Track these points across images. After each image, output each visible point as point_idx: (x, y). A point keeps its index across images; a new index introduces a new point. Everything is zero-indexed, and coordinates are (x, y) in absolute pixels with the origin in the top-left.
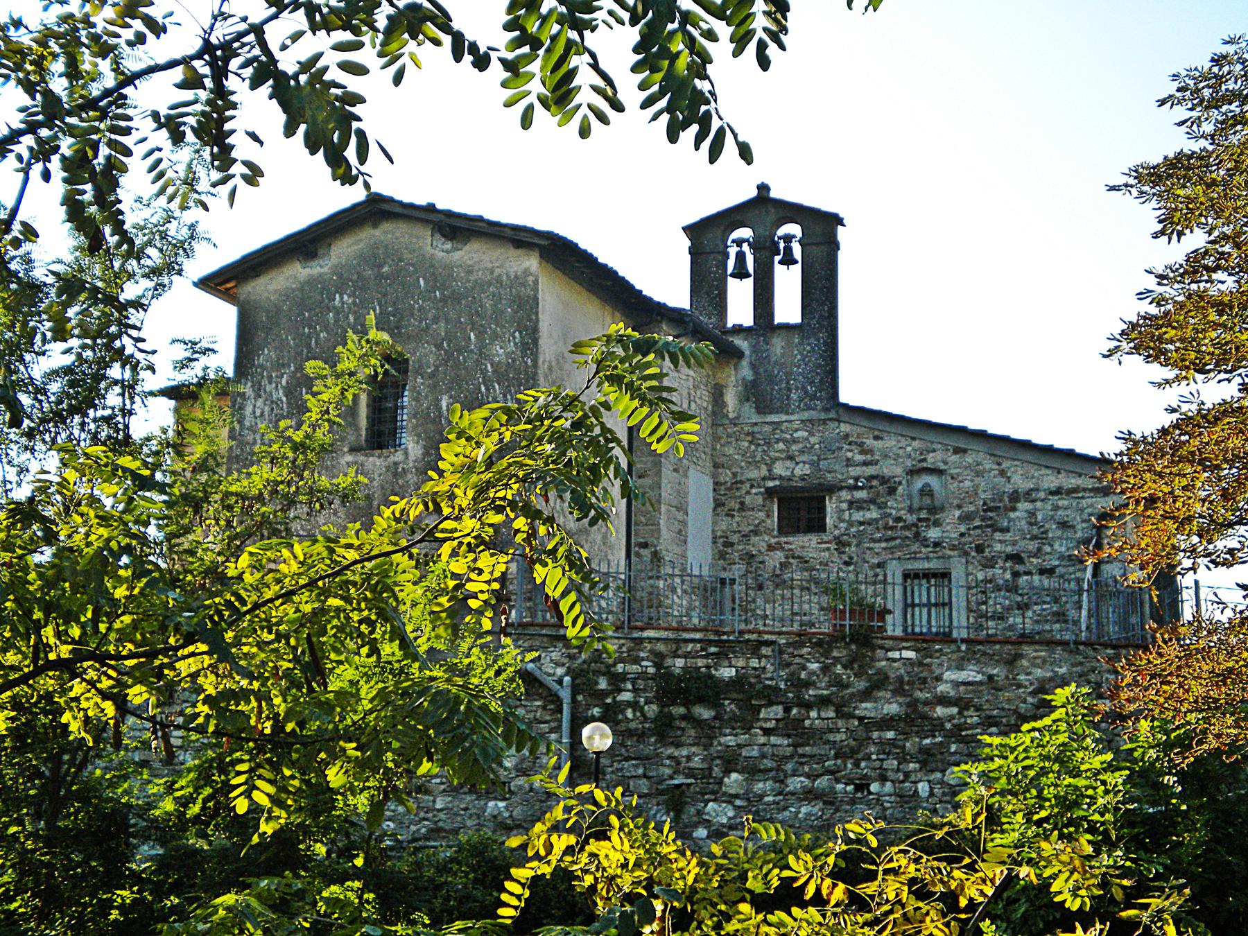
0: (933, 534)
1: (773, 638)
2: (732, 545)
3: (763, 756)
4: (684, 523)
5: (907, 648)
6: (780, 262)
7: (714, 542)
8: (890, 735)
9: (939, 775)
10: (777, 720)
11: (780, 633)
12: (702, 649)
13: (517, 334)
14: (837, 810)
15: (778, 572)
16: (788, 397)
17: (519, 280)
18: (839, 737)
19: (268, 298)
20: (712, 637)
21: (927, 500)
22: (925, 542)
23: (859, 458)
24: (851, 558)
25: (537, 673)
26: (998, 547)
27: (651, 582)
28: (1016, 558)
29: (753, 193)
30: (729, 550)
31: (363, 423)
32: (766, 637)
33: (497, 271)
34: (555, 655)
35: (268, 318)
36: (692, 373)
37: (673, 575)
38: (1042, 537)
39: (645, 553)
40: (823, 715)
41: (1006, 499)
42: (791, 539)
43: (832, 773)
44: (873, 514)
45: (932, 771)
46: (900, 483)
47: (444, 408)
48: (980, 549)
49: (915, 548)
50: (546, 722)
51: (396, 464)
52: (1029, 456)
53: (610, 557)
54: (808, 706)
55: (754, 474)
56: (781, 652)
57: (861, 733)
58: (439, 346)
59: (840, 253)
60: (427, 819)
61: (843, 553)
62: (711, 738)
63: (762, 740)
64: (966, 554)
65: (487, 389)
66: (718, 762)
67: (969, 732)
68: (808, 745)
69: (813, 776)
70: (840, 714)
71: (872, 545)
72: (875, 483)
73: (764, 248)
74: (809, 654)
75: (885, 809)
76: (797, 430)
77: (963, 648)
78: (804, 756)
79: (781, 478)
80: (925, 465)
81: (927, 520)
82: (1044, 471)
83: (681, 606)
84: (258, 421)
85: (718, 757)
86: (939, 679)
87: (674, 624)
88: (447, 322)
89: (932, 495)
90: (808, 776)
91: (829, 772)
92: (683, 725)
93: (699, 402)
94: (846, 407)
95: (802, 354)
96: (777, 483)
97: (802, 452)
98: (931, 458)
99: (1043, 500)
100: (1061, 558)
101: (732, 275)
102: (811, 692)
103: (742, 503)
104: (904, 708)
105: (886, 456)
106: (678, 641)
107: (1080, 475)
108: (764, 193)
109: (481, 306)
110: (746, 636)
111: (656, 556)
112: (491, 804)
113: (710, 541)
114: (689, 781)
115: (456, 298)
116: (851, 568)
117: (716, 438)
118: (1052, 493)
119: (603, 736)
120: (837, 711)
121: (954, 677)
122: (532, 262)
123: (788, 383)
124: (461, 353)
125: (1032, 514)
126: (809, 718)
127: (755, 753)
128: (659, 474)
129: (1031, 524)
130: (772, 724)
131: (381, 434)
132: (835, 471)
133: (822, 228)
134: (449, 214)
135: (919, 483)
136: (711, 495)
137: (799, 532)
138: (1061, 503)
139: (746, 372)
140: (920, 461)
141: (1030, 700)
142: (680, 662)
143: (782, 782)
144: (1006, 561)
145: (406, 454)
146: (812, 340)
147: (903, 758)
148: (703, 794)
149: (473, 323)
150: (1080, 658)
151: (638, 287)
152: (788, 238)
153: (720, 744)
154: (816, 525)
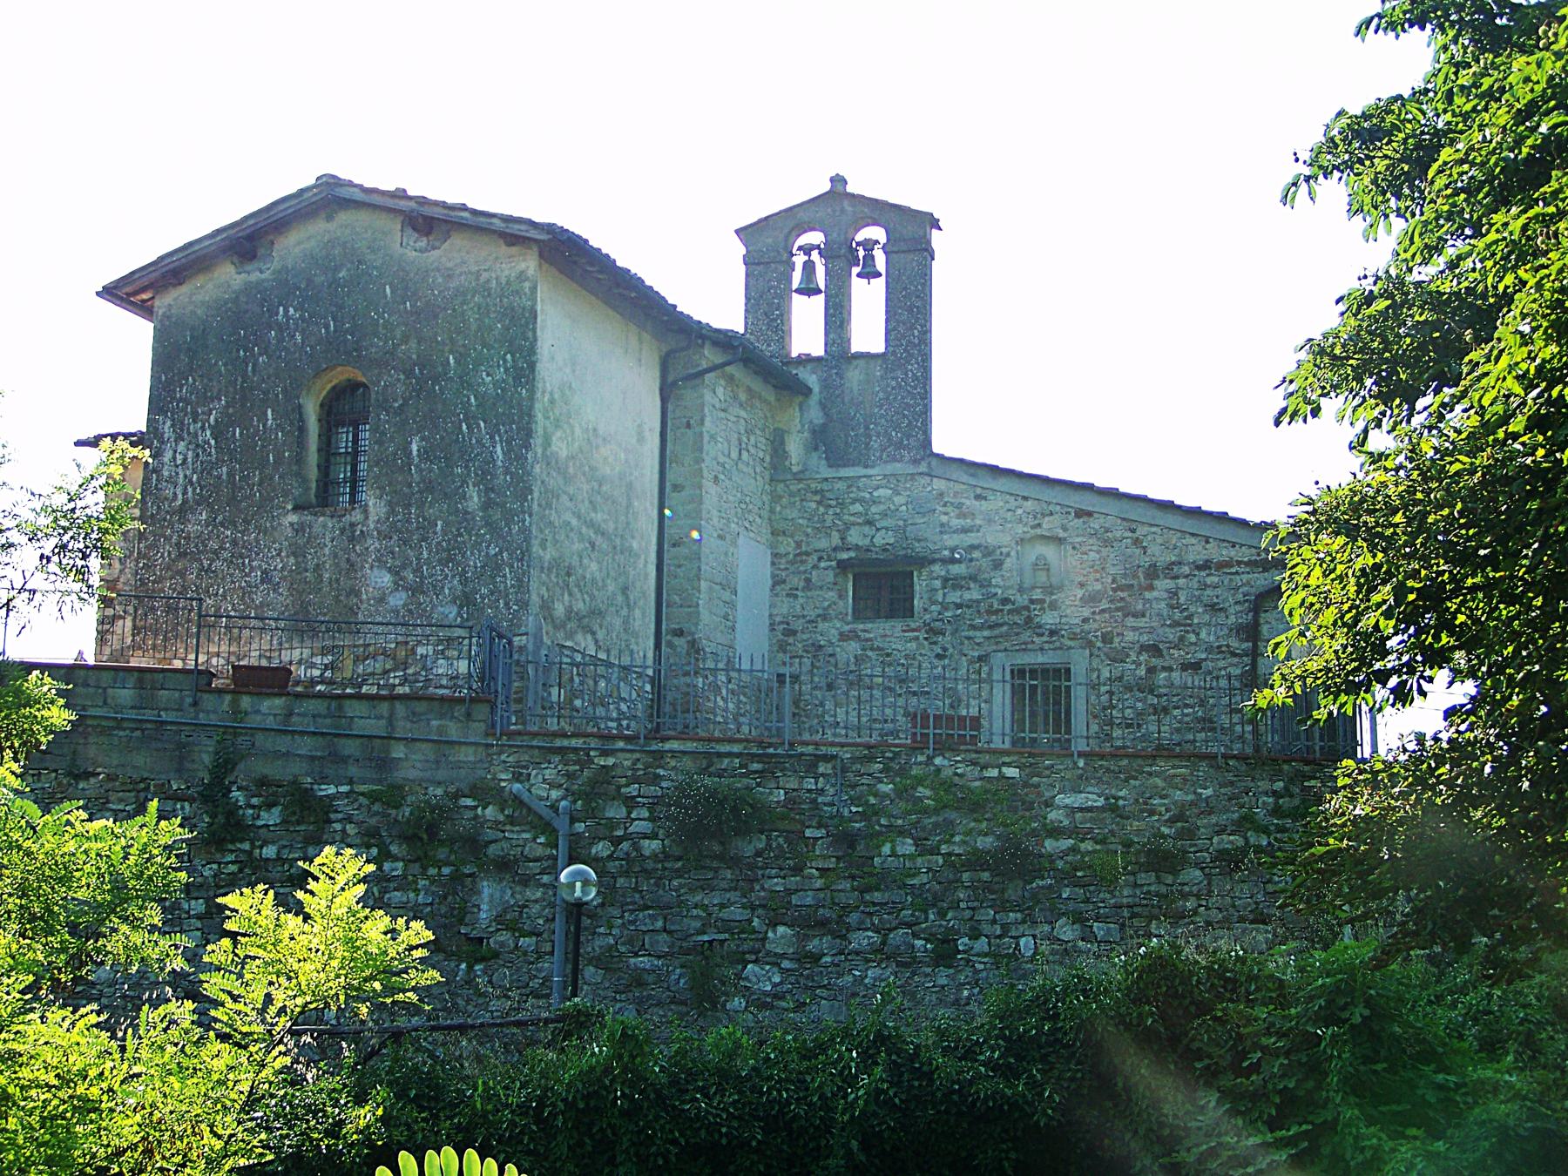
1: (834, 750)
2: (794, 633)
4: (732, 605)
5: (1008, 765)
6: (859, 275)
9: (1047, 928)
14: (914, 974)
15: (853, 667)
20: (754, 750)
22: (1038, 629)
24: (945, 649)
25: (525, 797)
26: (1130, 636)
27: (687, 679)
28: (1154, 650)
29: (827, 187)
30: (791, 640)
33: (485, 276)
34: (549, 773)
35: (192, 337)
36: (743, 414)
38: (1186, 624)
39: (680, 642)
42: (870, 626)
43: (909, 925)
46: (1008, 555)
47: (415, 453)
50: (536, 860)
51: (352, 525)
55: (823, 544)
56: (844, 770)
58: (409, 373)
59: (936, 265)
61: (935, 643)
66: (760, 911)
68: (878, 890)
71: (971, 633)
72: (976, 554)
75: (977, 972)
76: (877, 488)
77: (1081, 764)
80: (1039, 531)
81: (1042, 601)
83: (726, 710)
84: (180, 470)
86: (1049, 804)
87: (717, 734)
93: (752, 451)
94: (940, 457)
95: (885, 392)
96: (852, 554)
100: (1209, 649)
101: (798, 291)
103: (808, 581)
105: (990, 521)
108: (839, 187)
109: (464, 321)
110: (800, 749)
114: (722, 936)
117: (776, 498)
118: (1199, 568)
119: (586, 883)
122: (529, 263)
123: (867, 428)
127: (809, 901)
129: (1172, 607)
132: (926, 540)
133: (912, 234)
138: (1209, 580)
139: (815, 415)
143: (843, 938)
145: (366, 511)
150: (1230, 776)
151: (648, 283)
152: (869, 245)
153: (763, 888)
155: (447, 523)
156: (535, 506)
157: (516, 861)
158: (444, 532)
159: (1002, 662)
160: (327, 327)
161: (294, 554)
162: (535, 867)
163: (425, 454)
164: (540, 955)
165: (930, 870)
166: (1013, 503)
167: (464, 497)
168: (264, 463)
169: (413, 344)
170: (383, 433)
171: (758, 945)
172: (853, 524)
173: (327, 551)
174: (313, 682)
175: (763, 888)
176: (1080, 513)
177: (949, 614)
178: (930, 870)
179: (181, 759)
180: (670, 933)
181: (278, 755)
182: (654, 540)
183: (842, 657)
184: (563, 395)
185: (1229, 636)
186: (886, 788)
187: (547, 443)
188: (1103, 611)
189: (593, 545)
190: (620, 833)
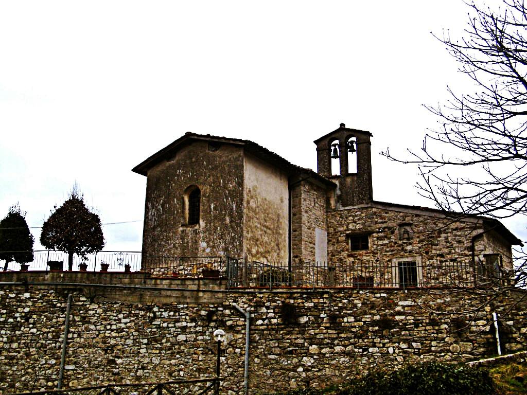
0: (409, 248)
1: (328, 290)
3: (325, 338)
5: (383, 293)
7: (328, 255)
14: (355, 360)
18: (354, 330)
22: (405, 251)
23: (380, 221)
24: (378, 258)
25: (237, 306)
26: (434, 252)
28: (442, 256)
29: (338, 127)
30: (334, 258)
31: (187, 216)
34: (244, 300)
36: (315, 193)
39: (297, 260)
40: (349, 320)
42: (355, 253)
44: (386, 241)
45: (395, 343)
46: (396, 229)
47: (212, 208)
48: (427, 253)
49: (402, 253)
51: (196, 230)
55: (341, 229)
58: (210, 186)
60: (196, 364)
61: (375, 257)
65: (226, 200)
67: (409, 326)
69: (345, 346)
71: (386, 253)
72: (386, 230)
74: (343, 296)
75: (375, 359)
76: (357, 212)
85: (307, 339)
86: (397, 305)
88: (213, 176)
90: (343, 346)
91: (351, 344)
95: (357, 183)
96: (350, 232)
97: (359, 220)
99: (450, 233)
100: (459, 255)
101: (333, 157)
103: (338, 240)
111: (301, 261)
116: (379, 262)
117: (328, 217)
118: (454, 230)
123: (353, 195)
124: (217, 187)
125: (446, 238)
126: (343, 322)
128: (301, 230)
129: (446, 242)
133: (364, 138)
136: (326, 238)
140: (403, 221)
143: (333, 348)
147: (382, 337)
148: (301, 354)
151: (289, 161)
152: (352, 142)
155: (221, 228)
156: (244, 221)
157: (235, 326)
158: (220, 230)
159: (395, 261)
160: (189, 174)
161: (182, 239)
162: (240, 328)
163: (215, 208)
164: (241, 355)
165: (359, 326)
166: (396, 214)
167: (225, 220)
168: (174, 214)
169: (212, 177)
170: (204, 203)
171: (306, 351)
172: (350, 223)
173: (190, 237)
174: (186, 275)
175: (308, 333)
176: (417, 215)
177: (379, 248)
178: (359, 326)
179: (141, 298)
180: (280, 348)
181: (167, 296)
182: (288, 230)
183: (348, 263)
184: (254, 189)
185: (465, 250)
186: (345, 301)
187: (248, 202)
188: (426, 244)
189: (266, 232)
190: (264, 317)
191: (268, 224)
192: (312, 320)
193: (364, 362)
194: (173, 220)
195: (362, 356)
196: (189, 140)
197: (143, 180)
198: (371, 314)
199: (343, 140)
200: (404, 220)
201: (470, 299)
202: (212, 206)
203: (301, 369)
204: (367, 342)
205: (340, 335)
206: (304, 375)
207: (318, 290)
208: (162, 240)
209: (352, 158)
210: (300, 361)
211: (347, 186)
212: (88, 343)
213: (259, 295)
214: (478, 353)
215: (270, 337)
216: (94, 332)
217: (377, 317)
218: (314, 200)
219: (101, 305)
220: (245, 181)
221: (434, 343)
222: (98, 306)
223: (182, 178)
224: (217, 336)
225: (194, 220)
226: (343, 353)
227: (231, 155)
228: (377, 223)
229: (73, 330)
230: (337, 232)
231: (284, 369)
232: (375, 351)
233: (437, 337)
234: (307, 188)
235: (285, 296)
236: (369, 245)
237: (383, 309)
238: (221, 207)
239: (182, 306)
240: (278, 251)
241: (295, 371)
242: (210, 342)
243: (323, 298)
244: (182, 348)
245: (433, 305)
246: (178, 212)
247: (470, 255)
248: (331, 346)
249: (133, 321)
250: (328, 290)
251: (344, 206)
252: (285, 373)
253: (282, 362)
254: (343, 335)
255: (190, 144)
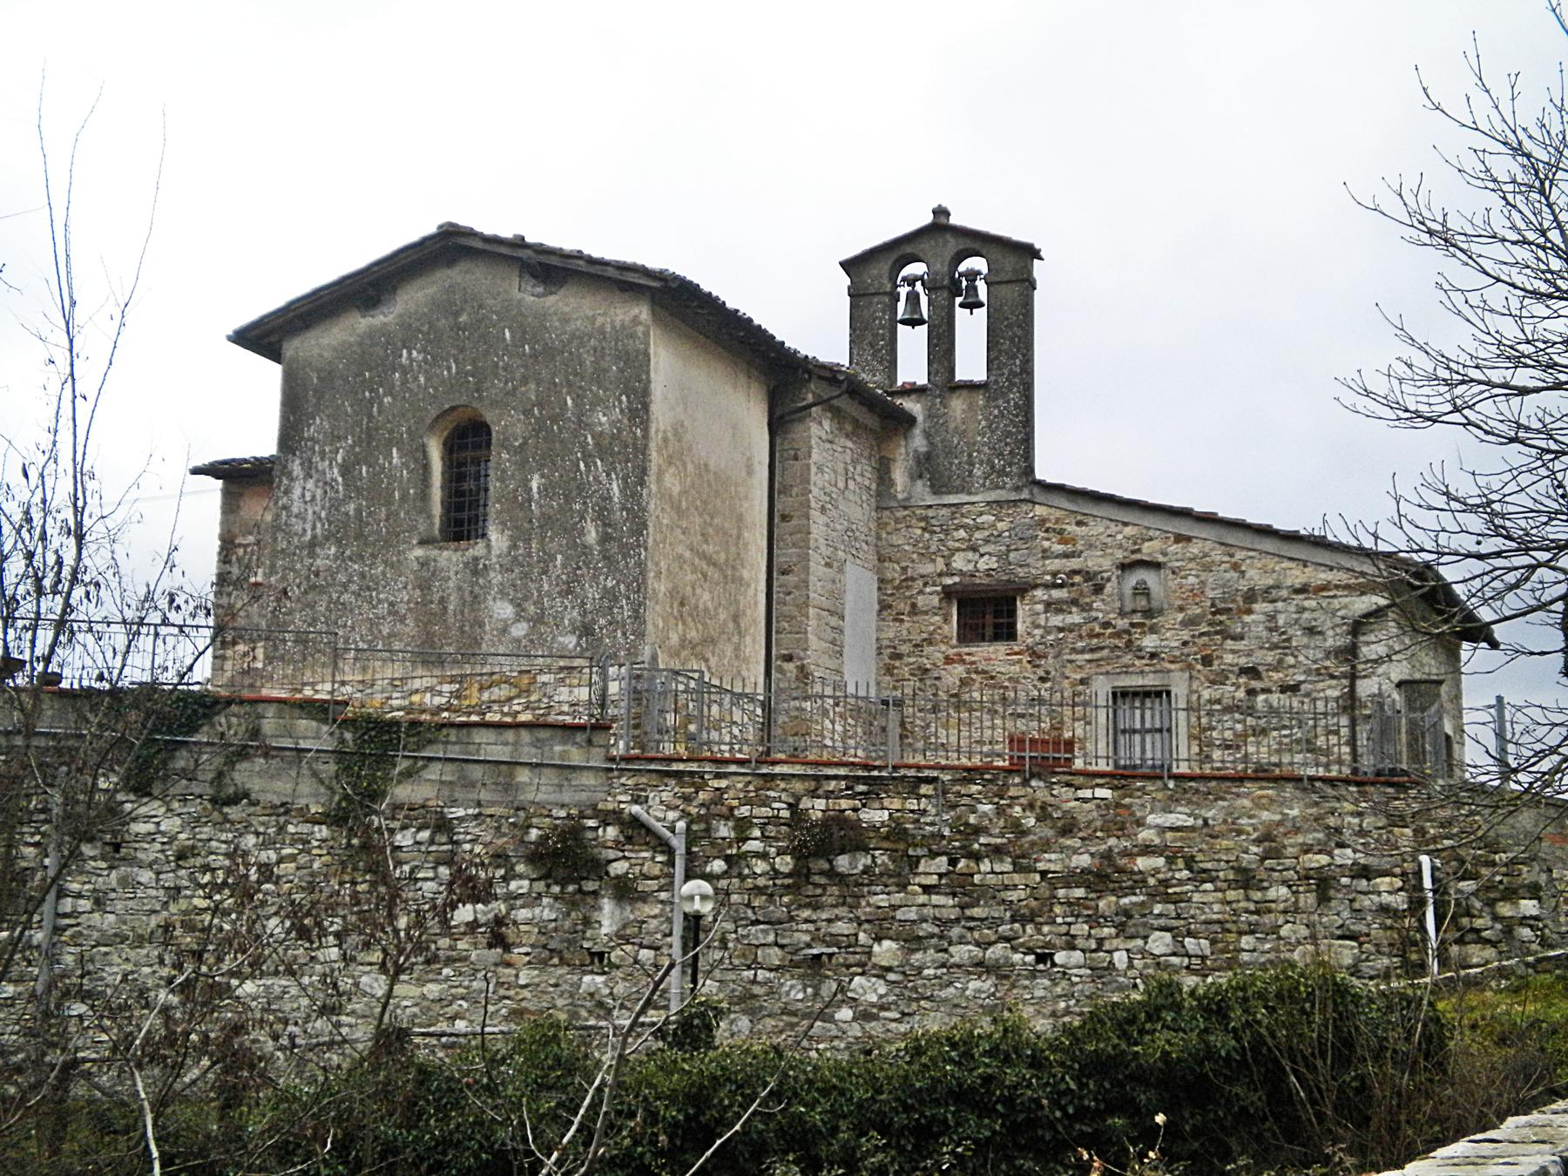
0: (1149, 642)
1: (935, 773)
2: (899, 656)
8: (1080, 892)
9: (1140, 942)
10: (941, 876)
11: (943, 768)
12: (847, 789)
13: (624, 398)
14: (1013, 986)
16: (971, 472)
17: (626, 332)
18: (1013, 896)
19: (321, 356)
20: (860, 773)
21: (1142, 603)
22: (1139, 653)
24: (1048, 673)
25: (644, 816)
26: (1229, 658)
27: (797, 703)
28: (1252, 672)
29: (928, 219)
30: (897, 663)
31: (437, 509)
32: (926, 773)
33: (600, 320)
36: (849, 444)
37: (822, 697)
38: (1285, 646)
40: (997, 868)
41: (1239, 599)
43: (1008, 940)
44: (1076, 618)
45: (1132, 937)
46: (1109, 580)
47: (535, 490)
48: (1207, 661)
51: (476, 559)
52: (1269, 545)
53: (745, 673)
54: (977, 857)
55: (928, 568)
56: (945, 793)
57: (1044, 891)
58: (528, 413)
60: (508, 998)
61: (1038, 666)
62: (857, 897)
63: (922, 899)
64: (1190, 667)
67: (1177, 890)
69: (985, 945)
70: (1018, 868)
71: (1073, 657)
72: (1077, 579)
73: (942, 288)
75: (1073, 984)
76: (981, 514)
78: (973, 919)
79: (961, 573)
81: (1142, 625)
82: (1286, 564)
85: (868, 921)
86: (1140, 823)
89: (1148, 595)
90: (978, 944)
92: (823, 881)
93: (859, 479)
95: (986, 419)
96: (957, 579)
97: (987, 541)
98: (1146, 547)
100: (1308, 672)
101: (904, 322)
102: (982, 840)
103: (914, 605)
104: (1097, 861)
105: (1091, 546)
106: (816, 778)
107: (1331, 569)
108: (942, 220)
110: (903, 772)
111: (804, 674)
112: (587, 979)
113: (874, 653)
115: (549, 353)
116: (1048, 685)
117: (881, 525)
118: (1298, 591)
120: (1014, 864)
121: (1160, 819)
122: (642, 312)
123: (970, 455)
125: (1272, 617)
128: (806, 569)
130: (933, 880)
131: (459, 523)
133: (1014, 261)
134: (540, 249)
135: (1133, 579)
137: (983, 640)
138: (1306, 604)
140: (1133, 552)
141: (1254, 849)
142: (820, 804)
143: (946, 951)
144: (1239, 676)
145: (488, 547)
146: (1000, 402)
147: (1095, 920)
148: (848, 967)
149: (569, 384)
150: (1315, 797)
151: (779, 338)
152: (972, 275)
153: (869, 904)
154: (1006, 632)
155: (567, 558)
156: (650, 541)
158: (564, 566)
160: (449, 369)
170: (504, 471)
172: (958, 550)
173: (451, 584)
175: (869, 904)
180: (782, 947)
182: (764, 568)
188: (1203, 634)
189: (705, 576)
191: (710, 549)
192: (883, 863)
193: (1039, 993)
194: (387, 520)
195: (1033, 975)
196: (451, 246)
197: (267, 376)
198: (1062, 849)
199: (941, 267)
200: (1139, 551)
201: (1360, 814)
202: (534, 485)
203: (845, 1014)
204: (1050, 933)
205: (968, 912)
206: (855, 1030)
207: (903, 772)
208: (345, 586)
209: (971, 330)
210: (842, 989)
211: (952, 426)
212: (133, 929)
213: (716, 783)
214: (1373, 973)
215: (749, 912)
216: (154, 893)
217: (1084, 860)
218: (846, 470)
219: (176, 805)
220: (654, 408)
221: (1247, 941)
222: (163, 810)
223: (422, 379)
224: (691, 898)
225: (463, 522)
226: (977, 965)
227: (605, 314)
228: (1046, 554)
229: (75, 887)
230: (913, 579)
231: (794, 1014)
232: (1073, 961)
233: (1257, 924)
234: (827, 427)
235: (798, 786)
236: (1019, 626)
237: (1099, 834)
238: (570, 489)
239: (461, 812)
240: (735, 639)
241: (831, 1019)
242: (556, 930)
243: (919, 797)
244: (461, 945)
245: (1250, 829)
246: (404, 498)
247: (1344, 676)
248: (943, 942)
249: (293, 858)
250: (935, 773)
251: (936, 491)
252: (797, 1024)
253: (788, 994)
254: (976, 912)
255: (451, 263)
